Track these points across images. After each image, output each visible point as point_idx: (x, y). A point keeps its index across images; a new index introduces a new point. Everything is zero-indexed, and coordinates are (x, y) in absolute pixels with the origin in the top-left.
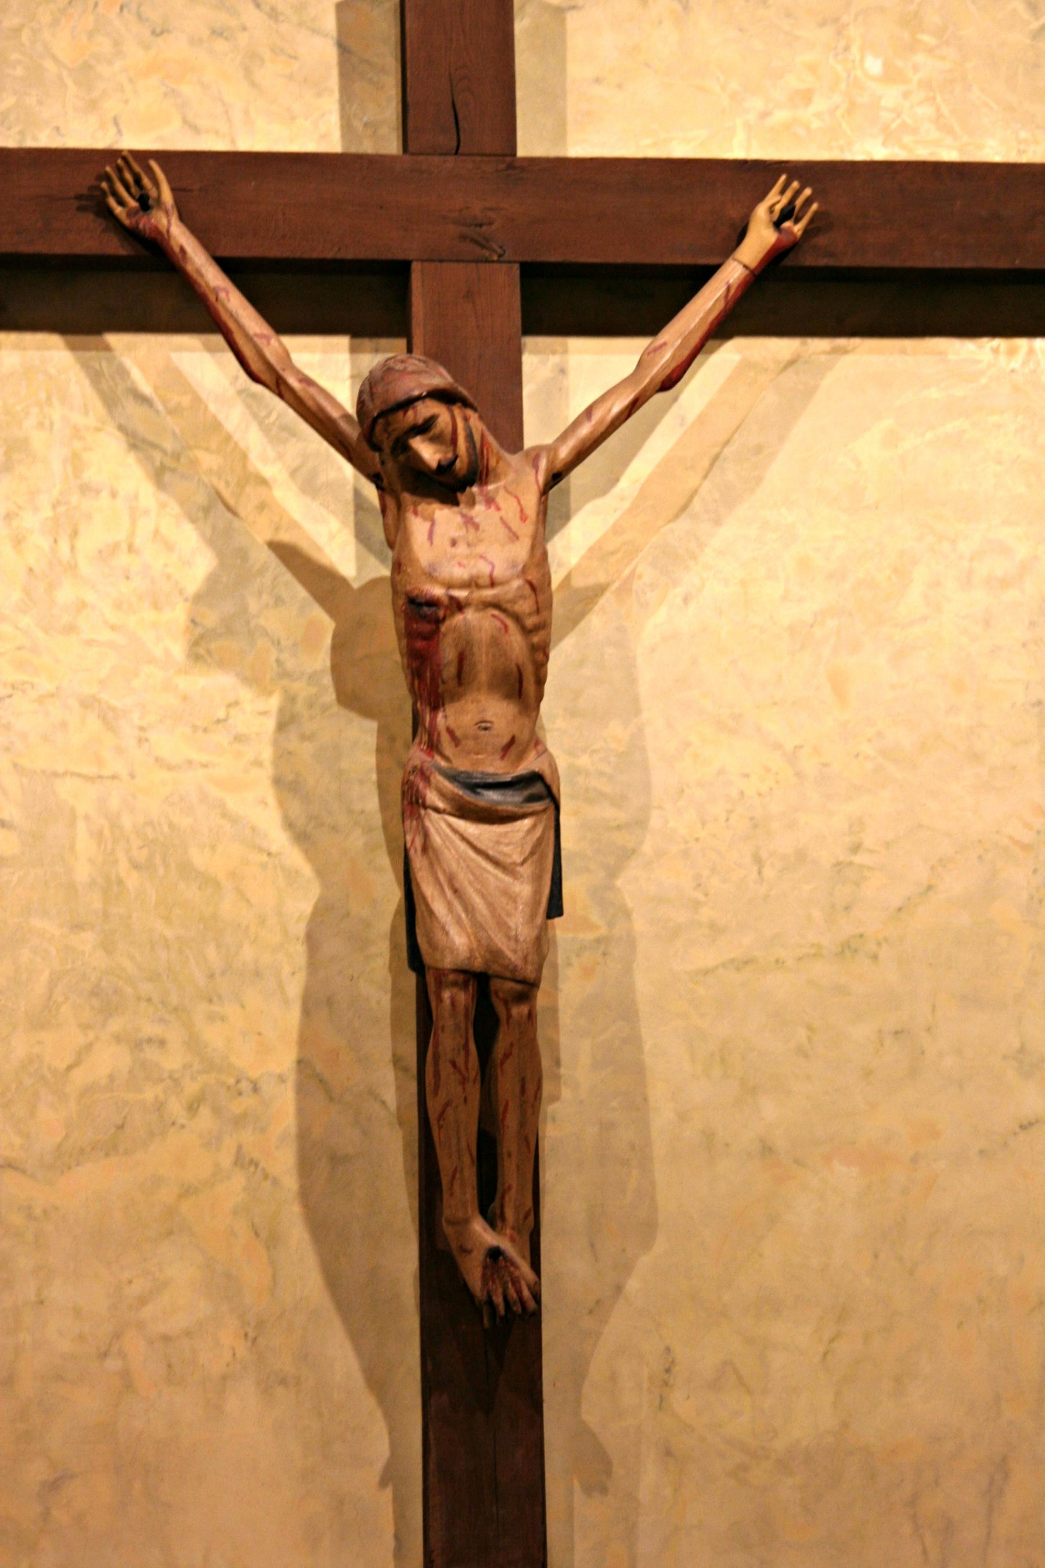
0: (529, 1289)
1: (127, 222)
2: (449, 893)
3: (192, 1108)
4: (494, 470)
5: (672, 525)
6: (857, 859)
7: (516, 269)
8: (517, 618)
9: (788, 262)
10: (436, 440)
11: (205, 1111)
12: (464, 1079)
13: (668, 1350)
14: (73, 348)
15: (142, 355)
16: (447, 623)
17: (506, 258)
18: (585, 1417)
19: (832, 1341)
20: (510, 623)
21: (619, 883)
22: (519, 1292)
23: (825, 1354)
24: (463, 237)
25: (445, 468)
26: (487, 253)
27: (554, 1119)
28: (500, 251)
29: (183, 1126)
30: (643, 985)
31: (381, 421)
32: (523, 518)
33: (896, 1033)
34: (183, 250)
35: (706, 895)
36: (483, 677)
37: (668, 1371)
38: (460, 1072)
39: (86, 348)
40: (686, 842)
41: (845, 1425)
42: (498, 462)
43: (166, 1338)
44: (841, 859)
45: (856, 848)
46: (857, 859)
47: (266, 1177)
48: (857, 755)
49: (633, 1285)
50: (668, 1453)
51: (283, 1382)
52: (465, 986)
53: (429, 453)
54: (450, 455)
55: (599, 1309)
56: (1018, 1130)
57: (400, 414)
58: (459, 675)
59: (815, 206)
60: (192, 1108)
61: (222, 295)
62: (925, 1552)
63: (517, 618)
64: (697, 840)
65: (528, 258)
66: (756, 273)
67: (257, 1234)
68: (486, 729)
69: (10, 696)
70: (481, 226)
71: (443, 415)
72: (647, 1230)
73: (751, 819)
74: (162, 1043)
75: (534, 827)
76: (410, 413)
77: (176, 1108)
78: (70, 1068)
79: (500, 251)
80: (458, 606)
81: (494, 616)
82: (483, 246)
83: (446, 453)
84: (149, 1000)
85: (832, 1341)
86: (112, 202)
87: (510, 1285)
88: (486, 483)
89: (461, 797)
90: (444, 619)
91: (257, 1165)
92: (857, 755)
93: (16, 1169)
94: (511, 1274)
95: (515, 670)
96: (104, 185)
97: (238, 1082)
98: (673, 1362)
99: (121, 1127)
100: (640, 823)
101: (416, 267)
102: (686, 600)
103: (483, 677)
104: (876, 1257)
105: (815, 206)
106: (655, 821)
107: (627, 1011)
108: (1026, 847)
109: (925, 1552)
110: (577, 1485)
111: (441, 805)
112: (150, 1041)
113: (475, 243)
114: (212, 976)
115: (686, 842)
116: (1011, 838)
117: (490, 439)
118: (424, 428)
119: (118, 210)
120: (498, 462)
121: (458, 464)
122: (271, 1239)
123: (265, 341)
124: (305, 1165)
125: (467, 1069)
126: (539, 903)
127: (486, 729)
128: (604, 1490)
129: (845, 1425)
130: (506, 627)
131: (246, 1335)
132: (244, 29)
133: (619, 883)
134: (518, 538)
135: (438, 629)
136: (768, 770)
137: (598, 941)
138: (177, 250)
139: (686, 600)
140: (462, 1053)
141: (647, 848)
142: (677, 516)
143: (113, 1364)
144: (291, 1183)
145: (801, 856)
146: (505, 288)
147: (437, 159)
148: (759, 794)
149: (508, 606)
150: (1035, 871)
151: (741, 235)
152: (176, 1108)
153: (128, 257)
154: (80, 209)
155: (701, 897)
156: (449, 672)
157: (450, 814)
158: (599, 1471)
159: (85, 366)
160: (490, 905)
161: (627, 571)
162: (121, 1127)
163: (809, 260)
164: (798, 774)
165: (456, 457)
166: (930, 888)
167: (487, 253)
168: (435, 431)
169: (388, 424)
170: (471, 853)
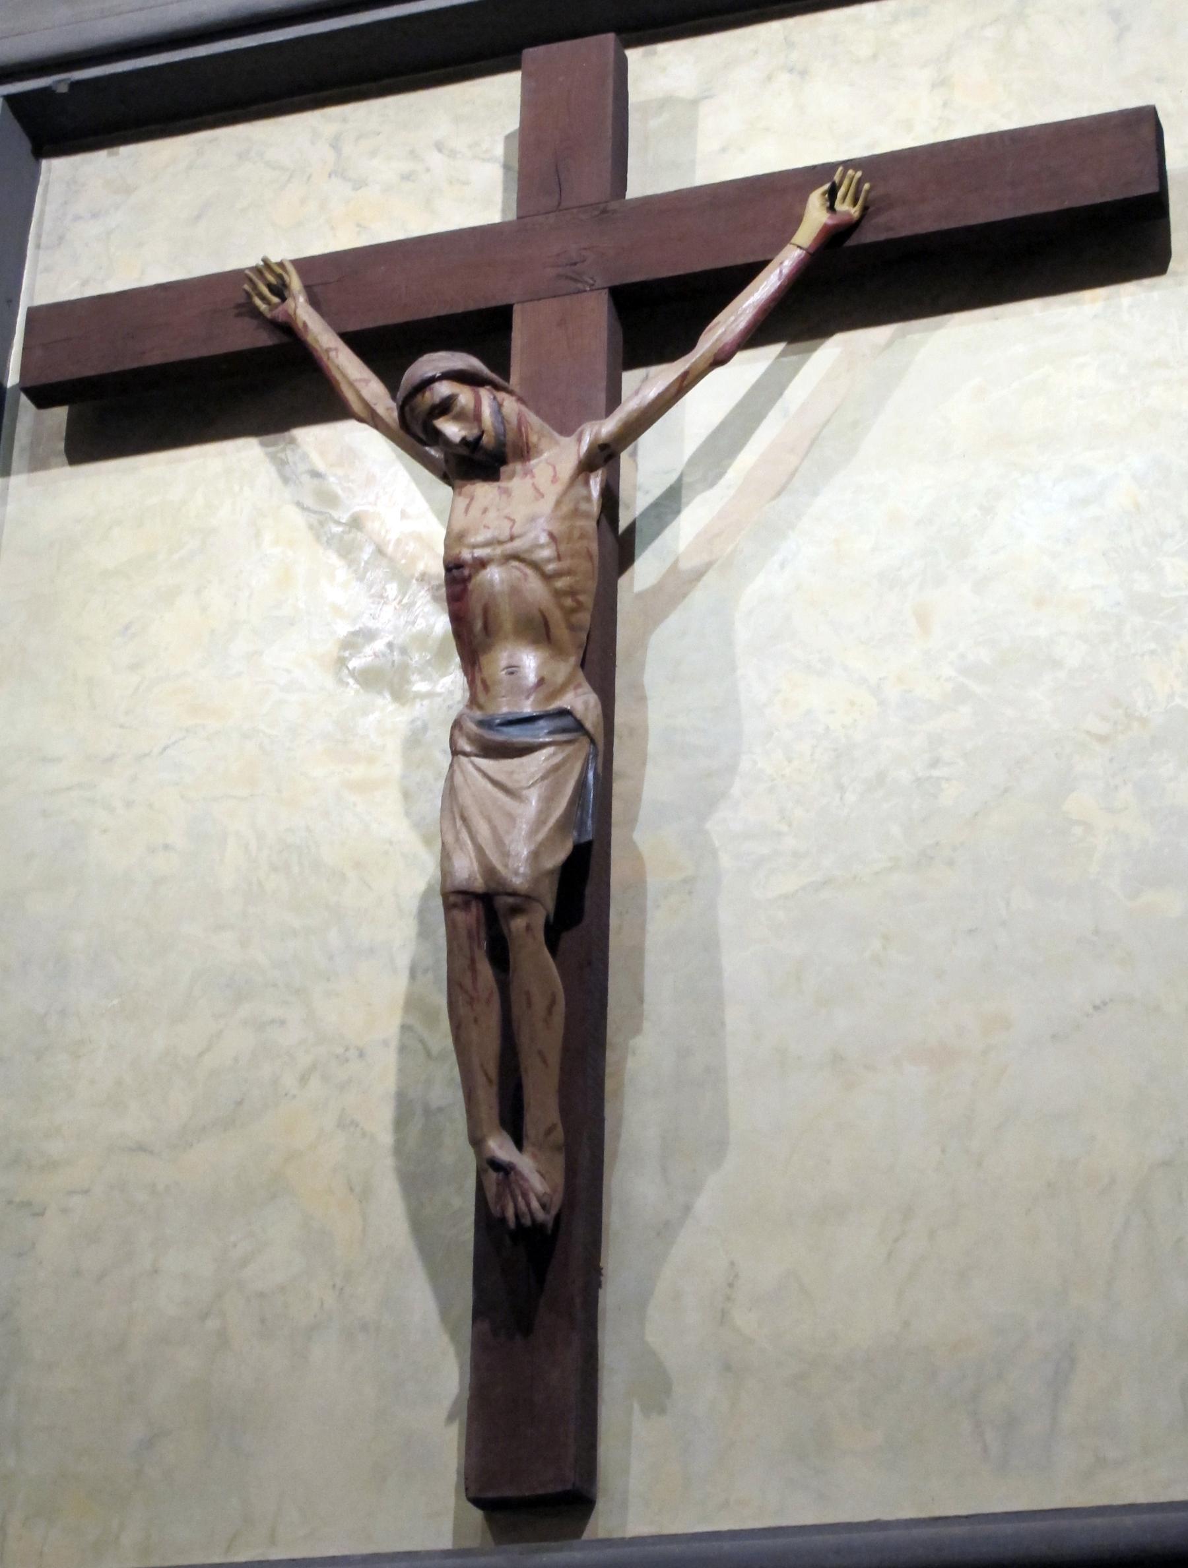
0: (539, 1200)
1: (269, 316)
2: (459, 823)
3: (304, 1080)
4: (536, 446)
5: (774, 503)
6: (936, 773)
7: (605, 296)
8: (536, 566)
9: (852, 242)
10: (460, 417)
11: (315, 1082)
12: (472, 998)
13: (732, 1264)
14: (263, 444)
15: (314, 440)
16: (473, 581)
17: (597, 286)
18: (649, 1338)
19: (896, 1240)
20: (529, 571)
21: (708, 826)
22: (528, 1205)
23: (890, 1254)
24: (559, 276)
25: (471, 445)
26: (580, 286)
27: (634, 1053)
28: (591, 282)
29: (294, 1096)
30: (725, 917)
31: (407, 408)
32: (555, 479)
33: (970, 931)
34: (305, 324)
35: (790, 825)
36: (508, 626)
37: (731, 1285)
38: (466, 992)
39: (274, 444)
40: (773, 780)
41: (907, 1324)
42: (539, 439)
43: (261, 1295)
44: (920, 774)
45: (935, 763)
46: (936, 773)
47: (364, 1135)
48: (938, 679)
49: (702, 1203)
50: (727, 1368)
51: (364, 1327)
52: (466, 906)
53: (452, 430)
54: (476, 432)
55: (666, 1231)
56: (1091, 1011)
57: (419, 397)
58: (486, 627)
59: (867, 186)
60: (304, 1080)
61: (333, 354)
62: (985, 1449)
63: (536, 566)
64: (783, 776)
65: (617, 283)
66: (811, 251)
67: (351, 1190)
68: (512, 673)
69: (184, 738)
70: (575, 264)
71: (465, 396)
72: (718, 1149)
73: (835, 750)
74: (283, 1023)
75: (554, 754)
76: (428, 394)
77: (289, 1081)
78: (201, 1054)
79: (591, 282)
80: (482, 564)
81: (516, 568)
82: (576, 280)
83: (471, 429)
84: (275, 985)
85: (896, 1240)
86: (258, 302)
87: (520, 1198)
88: (529, 460)
89: (481, 736)
90: (470, 578)
91: (357, 1126)
92: (938, 679)
93: (145, 1150)
94: (520, 1186)
95: (539, 615)
96: (247, 287)
97: (347, 1049)
98: (736, 1276)
99: (240, 1103)
100: (731, 769)
101: (515, 308)
102: (782, 566)
103: (508, 626)
104: (943, 1151)
105: (867, 186)
106: (745, 764)
107: (710, 944)
108: (1103, 739)
109: (985, 1449)
110: (636, 1406)
111: (468, 748)
112: (272, 1022)
113: (570, 280)
114: (331, 958)
115: (773, 780)
116: (1088, 733)
117: (533, 419)
118: (445, 407)
119: (263, 307)
120: (539, 439)
121: (485, 439)
122: (364, 1193)
123: (363, 384)
124: (401, 1122)
125: (475, 989)
126: (544, 822)
127: (512, 673)
128: (662, 1411)
129: (907, 1324)
130: (526, 575)
131: (334, 1286)
132: (428, 170)
133: (708, 826)
134: (543, 496)
135: (465, 590)
136: (852, 703)
137: (685, 881)
138: (300, 325)
139: (782, 566)
140: (469, 974)
141: (736, 791)
142: (779, 494)
143: (212, 1324)
144: (386, 1138)
145: (881, 777)
146: (596, 313)
147: (541, 219)
148: (844, 726)
149: (526, 556)
150: (1111, 760)
151: (799, 220)
152: (289, 1081)
153: (274, 346)
154: (239, 315)
155: (784, 828)
156: (479, 625)
157: (477, 755)
158: (657, 1391)
159: (273, 458)
160: (494, 829)
161: (730, 548)
162: (240, 1103)
163: (868, 236)
164: (881, 703)
165: (483, 432)
166: (1006, 790)
167: (580, 286)
168: (456, 410)
169: (412, 410)
170: (489, 786)
